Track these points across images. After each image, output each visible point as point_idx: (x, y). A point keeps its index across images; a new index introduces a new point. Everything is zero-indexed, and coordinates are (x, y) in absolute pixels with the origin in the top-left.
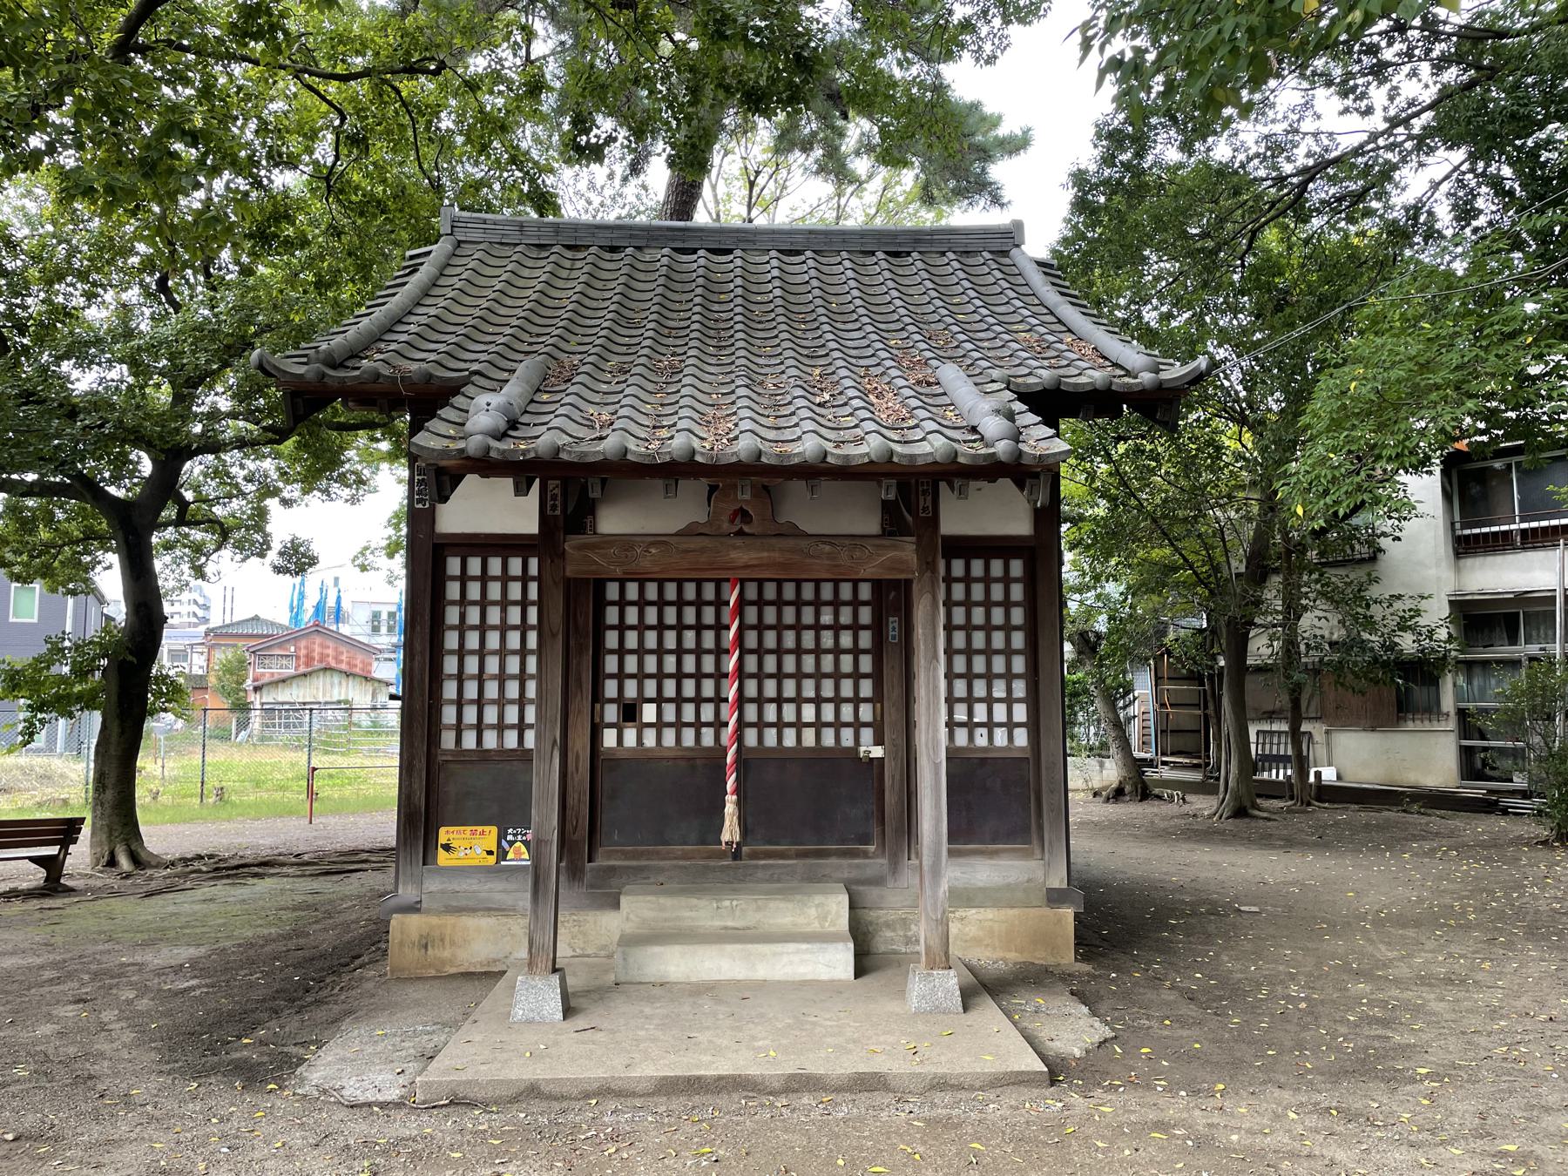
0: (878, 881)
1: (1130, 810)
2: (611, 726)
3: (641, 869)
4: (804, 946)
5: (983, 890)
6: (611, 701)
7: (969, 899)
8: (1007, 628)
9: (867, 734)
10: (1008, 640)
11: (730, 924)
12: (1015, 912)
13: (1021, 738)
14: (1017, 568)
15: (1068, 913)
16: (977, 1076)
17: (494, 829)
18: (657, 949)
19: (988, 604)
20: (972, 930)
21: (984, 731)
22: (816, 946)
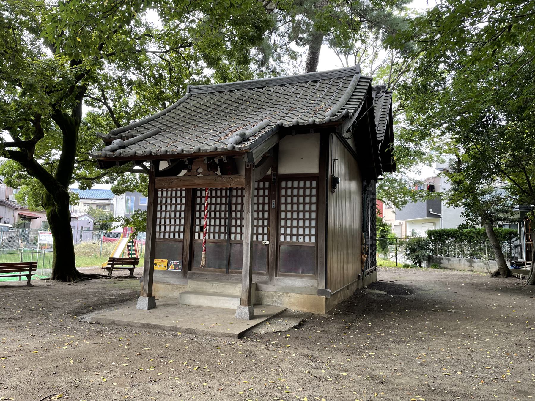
0: (265, 283)
1: (501, 281)
2: (197, 232)
3: (201, 274)
4: (227, 298)
5: (298, 288)
6: (197, 225)
7: (293, 291)
8: (311, 204)
9: (266, 237)
10: (310, 207)
11: (215, 291)
12: (307, 296)
13: (313, 239)
14: (314, 184)
15: (324, 298)
16: (218, 333)
17: (167, 260)
18: (188, 295)
19: (304, 196)
20: (292, 300)
21: (302, 237)
22: (230, 298)
